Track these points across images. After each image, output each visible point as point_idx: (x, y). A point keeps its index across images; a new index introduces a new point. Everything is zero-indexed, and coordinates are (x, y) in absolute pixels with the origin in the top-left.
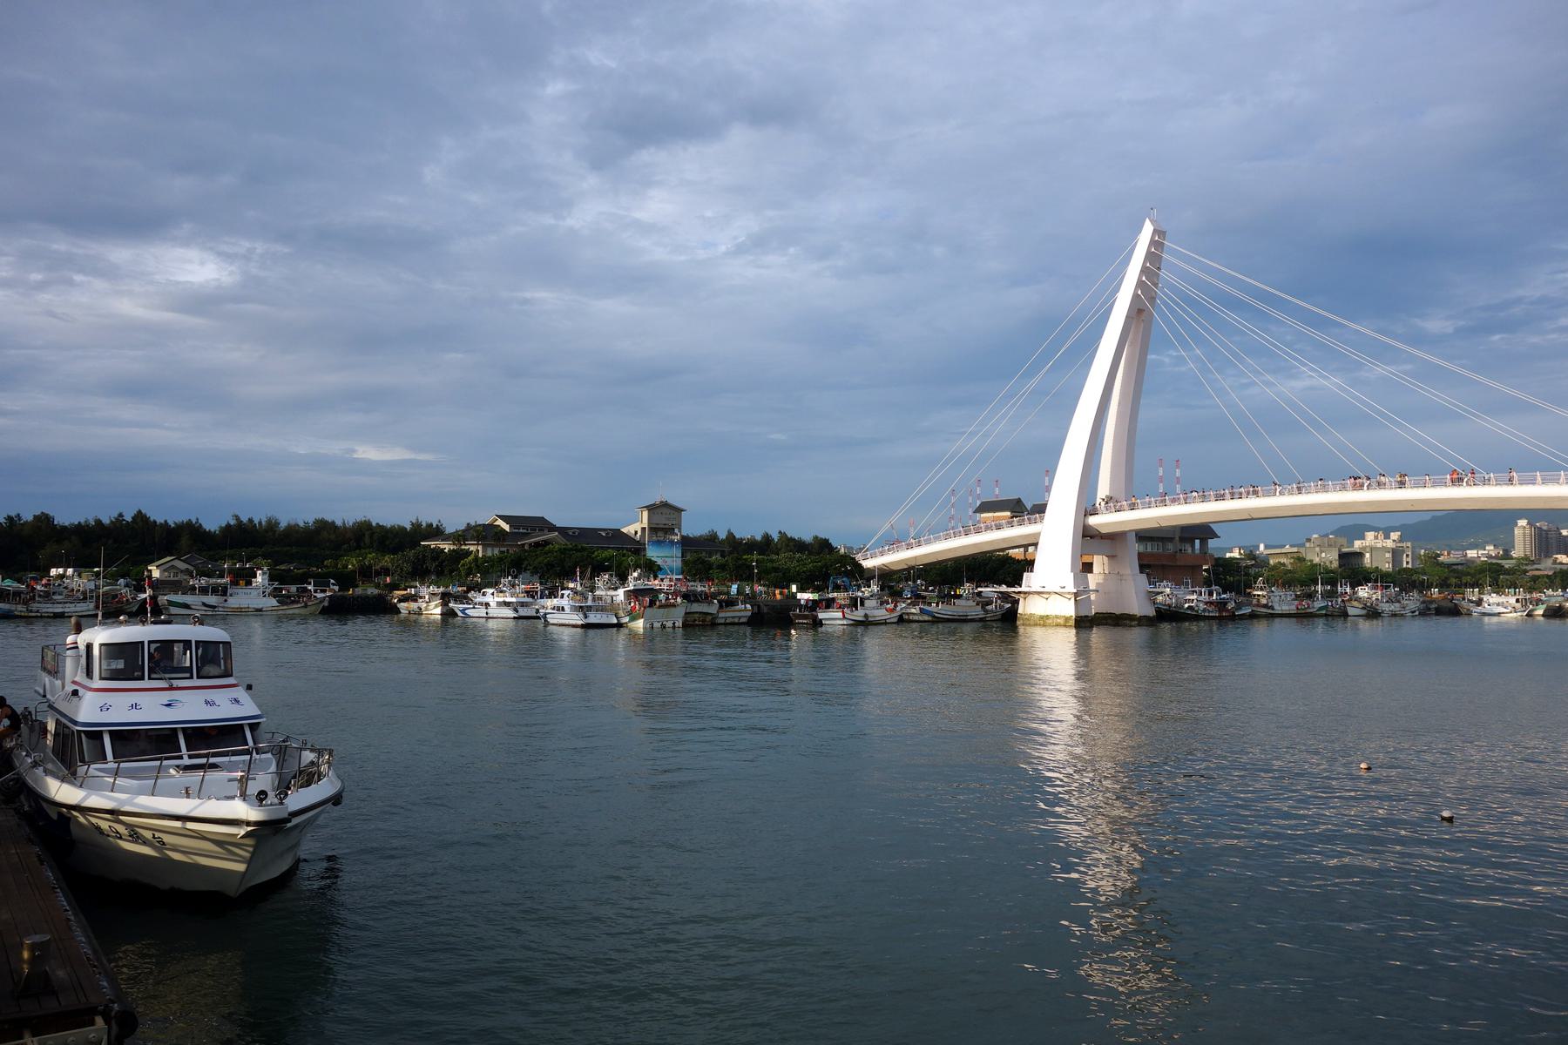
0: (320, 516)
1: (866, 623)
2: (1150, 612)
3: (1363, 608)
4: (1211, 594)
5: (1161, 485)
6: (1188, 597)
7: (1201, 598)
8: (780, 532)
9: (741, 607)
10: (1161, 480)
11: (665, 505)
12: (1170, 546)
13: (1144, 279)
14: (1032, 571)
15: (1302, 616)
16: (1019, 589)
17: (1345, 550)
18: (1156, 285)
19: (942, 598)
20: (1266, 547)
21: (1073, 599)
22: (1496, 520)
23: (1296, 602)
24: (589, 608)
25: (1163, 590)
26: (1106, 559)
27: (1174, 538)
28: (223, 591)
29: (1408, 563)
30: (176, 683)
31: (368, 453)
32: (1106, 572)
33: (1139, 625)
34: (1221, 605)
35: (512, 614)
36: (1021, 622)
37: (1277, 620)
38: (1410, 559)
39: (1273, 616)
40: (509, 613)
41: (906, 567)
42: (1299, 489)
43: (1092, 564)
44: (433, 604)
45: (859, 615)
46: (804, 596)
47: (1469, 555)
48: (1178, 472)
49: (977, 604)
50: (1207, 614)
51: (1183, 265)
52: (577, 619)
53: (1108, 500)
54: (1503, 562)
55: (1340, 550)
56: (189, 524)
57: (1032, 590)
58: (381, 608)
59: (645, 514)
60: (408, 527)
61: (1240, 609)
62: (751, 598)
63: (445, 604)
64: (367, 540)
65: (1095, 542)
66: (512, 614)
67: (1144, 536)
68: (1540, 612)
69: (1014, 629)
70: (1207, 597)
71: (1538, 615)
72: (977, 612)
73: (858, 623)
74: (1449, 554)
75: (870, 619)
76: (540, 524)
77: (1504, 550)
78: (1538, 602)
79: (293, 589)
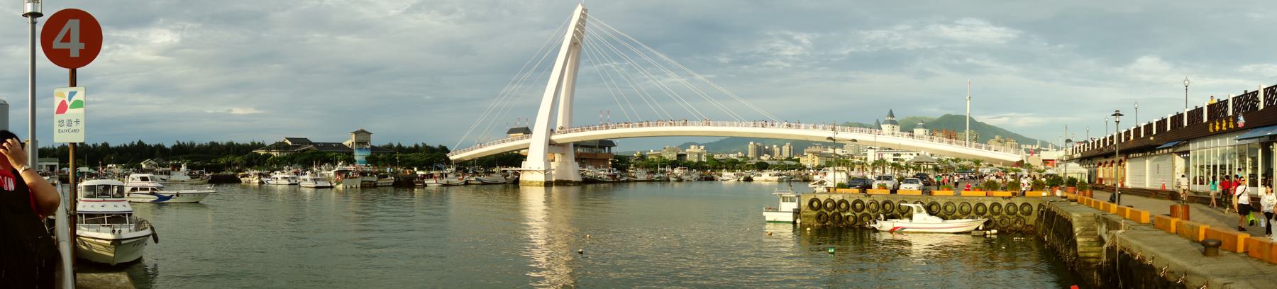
0: (212, 141)
1: (448, 185)
2: (579, 179)
4: (610, 171)
9: (389, 178)
11: (363, 131)
12: (594, 150)
15: (650, 181)
16: (520, 169)
18: (583, 32)
22: (741, 141)
24: (318, 179)
28: (168, 173)
30: (106, 199)
31: (237, 111)
33: (574, 185)
34: (614, 176)
35: (288, 183)
39: (636, 181)
40: (287, 182)
44: (255, 178)
45: (444, 181)
46: (420, 173)
48: (609, 117)
52: (313, 184)
53: (562, 128)
56: (159, 145)
58: (234, 180)
59: (354, 135)
60: (250, 144)
62: (395, 174)
63: (260, 178)
64: (232, 150)
65: (555, 148)
66: (288, 183)
67: (576, 145)
68: (742, 179)
72: (502, 180)
73: (444, 185)
76: (305, 141)
78: (742, 175)
79: (197, 172)
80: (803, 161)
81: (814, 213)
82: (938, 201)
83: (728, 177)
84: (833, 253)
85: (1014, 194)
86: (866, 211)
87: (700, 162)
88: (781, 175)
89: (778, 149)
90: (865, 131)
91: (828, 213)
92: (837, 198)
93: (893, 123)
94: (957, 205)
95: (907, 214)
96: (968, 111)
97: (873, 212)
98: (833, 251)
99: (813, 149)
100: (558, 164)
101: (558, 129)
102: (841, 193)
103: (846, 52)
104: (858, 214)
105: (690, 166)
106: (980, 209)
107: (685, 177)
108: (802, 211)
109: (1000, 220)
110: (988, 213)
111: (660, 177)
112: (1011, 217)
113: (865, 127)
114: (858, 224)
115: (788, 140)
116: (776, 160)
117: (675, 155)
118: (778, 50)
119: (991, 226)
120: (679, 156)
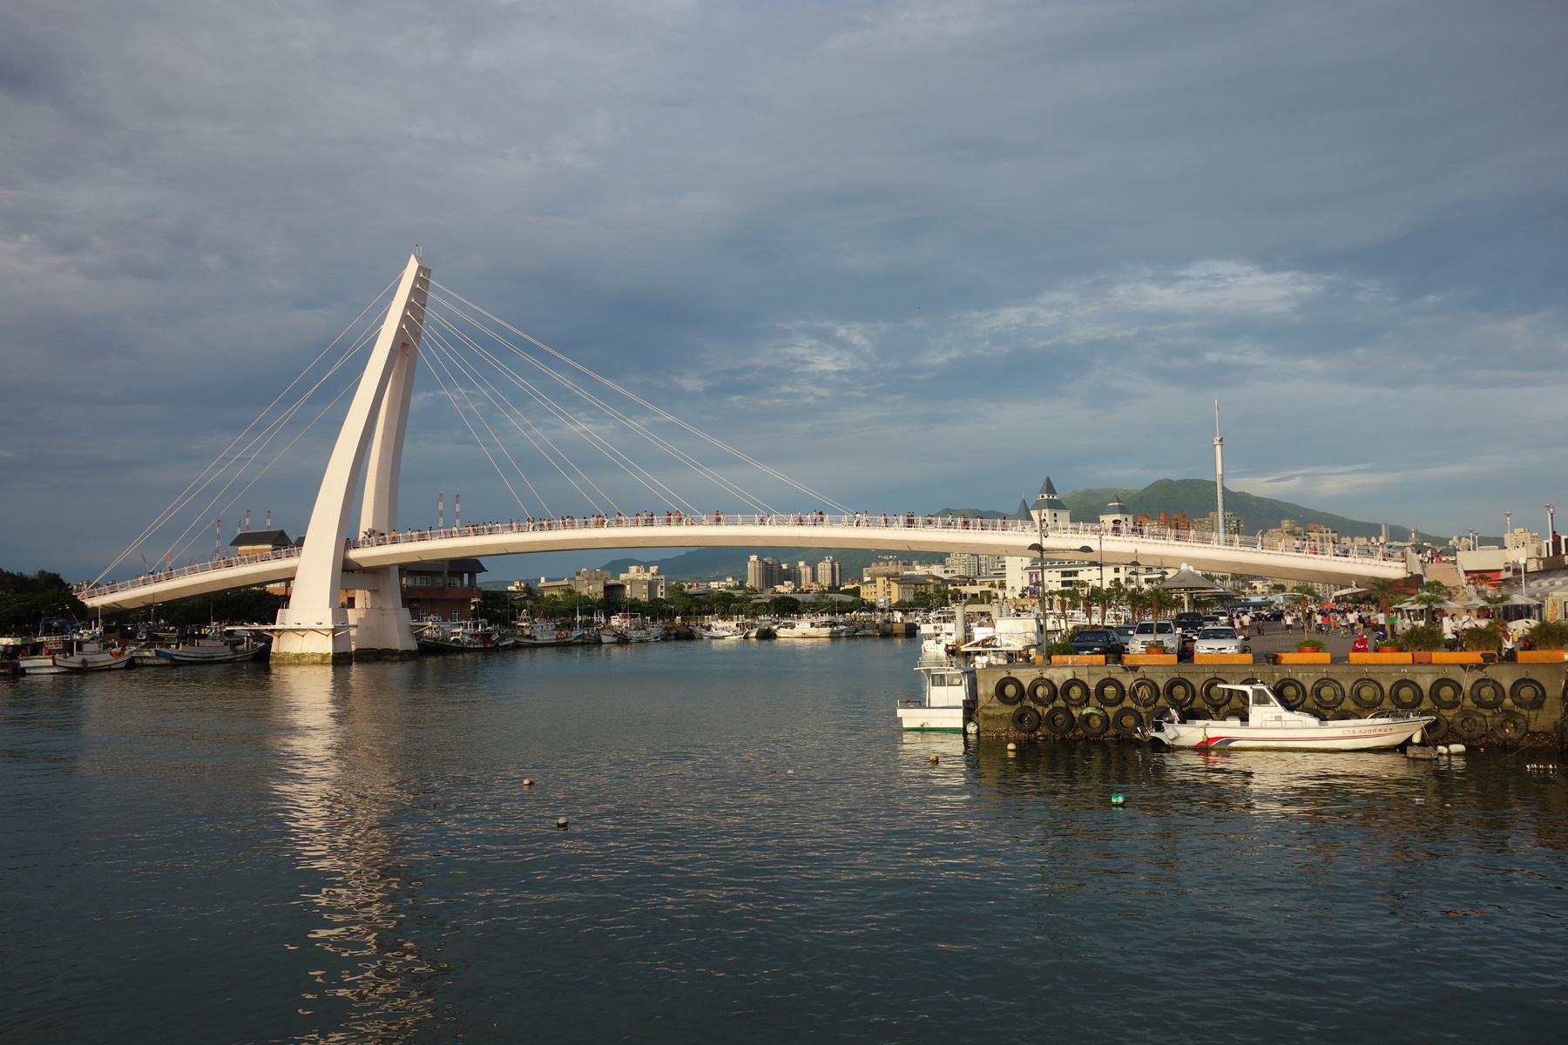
1: (84, 671)
2: (412, 645)
3: (614, 636)
4: (476, 627)
5: (441, 519)
6: (454, 631)
7: (466, 631)
10: (441, 513)
12: (439, 580)
13: (409, 314)
15: (562, 645)
16: (272, 627)
17: (612, 582)
18: (421, 321)
19: (183, 638)
20: (547, 580)
21: (331, 635)
22: (731, 556)
23: (556, 632)
25: (425, 623)
26: (368, 593)
27: (443, 572)
29: (662, 594)
32: (369, 606)
34: (486, 637)
36: (274, 662)
37: (539, 650)
38: (663, 591)
41: (143, 605)
42: (966, 523)
43: (354, 598)
45: (75, 660)
47: (712, 586)
49: (226, 644)
50: (471, 646)
51: (455, 310)
53: (371, 533)
54: (734, 592)
55: (605, 583)
57: (286, 627)
61: (504, 640)
67: (408, 569)
69: (268, 670)
70: (472, 629)
71: (752, 637)
72: (227, 652)
73: (73, 671)
74: (698, 585)
75: (89, 665)
77: (740, 582)
78: (752, 626)
80: (867, 594)
81: (1009, 710)
82: (1299, 677)
83: (725, 631)
84: (1122, 805)
85: (1488, 659)
86: (1128, 703)
87: (654, 602)
88: (835, 624)
89: (809, 570)
90: (975, 525)
91: (1040, 709)
92: (1058, 676)
93: (1055, 505)
94: (1347, 685)
95: (1227, 708)
96: (1219, 471)
97: (1146, 706)
98: (1120, 799)
99: (882, 568)
100: (362, 614)
101: (361, 536)
102: (1065, 666)
103: (942, 359)
104: (1111, 711)
105: (634, 608)
106: (1406, 694)
107: (634, 634)
108: (981, 705)
109: (1458, 720)
110: (1427, 704)
111: (582, 636)
112: (1488, 713)
113: (993, 515)
114: (1112, 731)
115: (751, 550)
116: (808, 592)
117: (600, 588)
118: (805, 363)
119: (1439, 734)
120: (609, 589)
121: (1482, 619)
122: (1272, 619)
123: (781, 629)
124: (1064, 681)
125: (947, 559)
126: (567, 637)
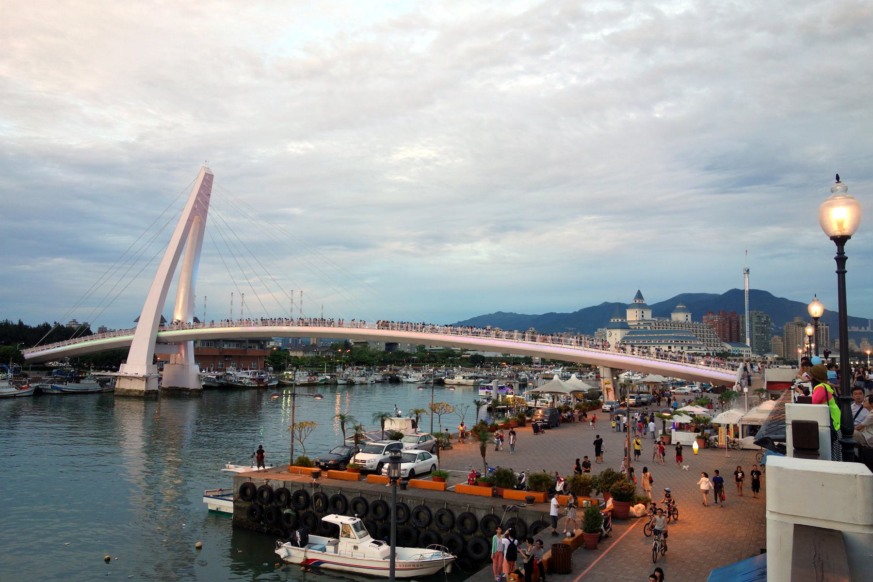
8: (55, 323)
14: (125, 363)
23: (308, 378)
34: (261, 380)
88: (477, 378)
107: (357, 379)
121: (400, 495)
122: (710, 392)
123: (447, 379)
124: (278, 488)
125: (595, 332)
126: (315, 380)
